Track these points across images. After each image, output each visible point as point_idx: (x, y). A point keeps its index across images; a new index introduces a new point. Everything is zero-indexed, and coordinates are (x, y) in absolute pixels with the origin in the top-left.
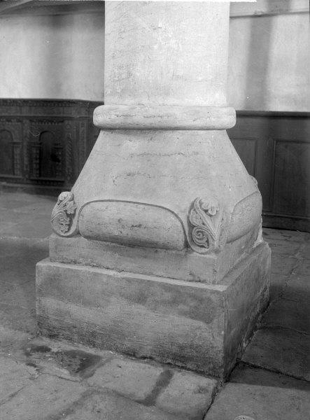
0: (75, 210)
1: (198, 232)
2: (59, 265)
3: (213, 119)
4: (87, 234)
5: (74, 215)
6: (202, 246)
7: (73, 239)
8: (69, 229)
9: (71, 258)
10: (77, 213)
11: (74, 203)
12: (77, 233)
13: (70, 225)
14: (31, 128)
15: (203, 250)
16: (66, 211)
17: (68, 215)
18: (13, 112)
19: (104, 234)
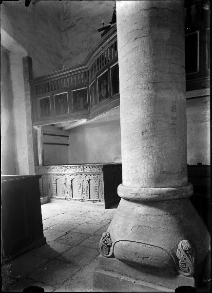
0: (111, 244)
1: (182, 264)
2: (118, 276)
3: (184, 194)
4: (118, 257)
5: (111, 246)
6: (186, 272)
7: (111, 259)
8: (109, 253)
9: (110, 268)
10: (113, 245)
11: (111, 239)
12: (113, 256)
13: (109, 251)
14: (71, 211)
15: (186, 274)
16: (107, 244)
17: (108, 246)
18: (116, 55)
19: (128, 260)
